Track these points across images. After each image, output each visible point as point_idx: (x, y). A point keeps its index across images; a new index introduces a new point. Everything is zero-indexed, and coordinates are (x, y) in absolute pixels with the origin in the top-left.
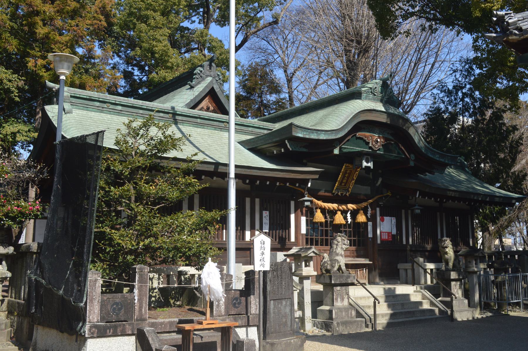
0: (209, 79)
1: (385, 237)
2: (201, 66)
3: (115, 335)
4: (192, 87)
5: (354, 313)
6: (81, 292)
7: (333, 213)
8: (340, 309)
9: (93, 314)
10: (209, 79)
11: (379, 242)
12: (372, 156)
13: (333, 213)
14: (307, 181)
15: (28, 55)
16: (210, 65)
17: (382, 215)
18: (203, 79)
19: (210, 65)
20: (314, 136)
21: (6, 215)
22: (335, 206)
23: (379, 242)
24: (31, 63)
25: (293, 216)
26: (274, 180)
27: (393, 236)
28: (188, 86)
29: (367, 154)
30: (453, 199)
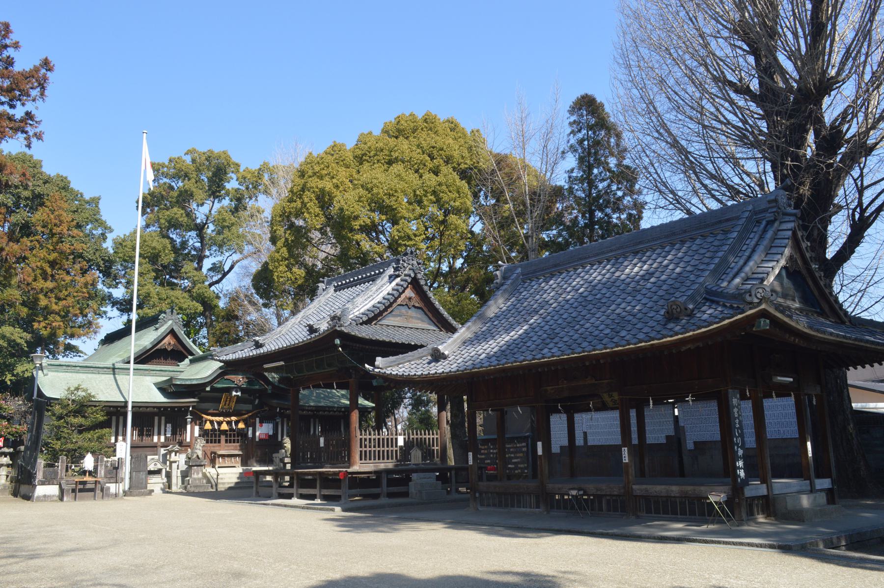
0: (170, 322)
1: (263, 437)
2: (165, 313)
3: (49, 484)
4: (157, 329)
5: (205, 481)
6: (34, 467)
7: (219, 423)
8: (195, 479)
9: (40, 476)
10: (170, 322)
11: (257, 440)
12: (238, 388)
13: (219, 423)
14: (189, 407)
15: (34, 321)
16: (172, 312)
17: (261, 422)
18: (166, 322)
19: (172, 312)
20: (187, 383)
21: (9, 433)
22: (221, 419)
23: (257, 440)
24: (36, 325)
25: (189, 427)
26: (172, 408)
27: (270, 436)
28: (153, 328)
29: (234, 388)
30: (308, 411)
